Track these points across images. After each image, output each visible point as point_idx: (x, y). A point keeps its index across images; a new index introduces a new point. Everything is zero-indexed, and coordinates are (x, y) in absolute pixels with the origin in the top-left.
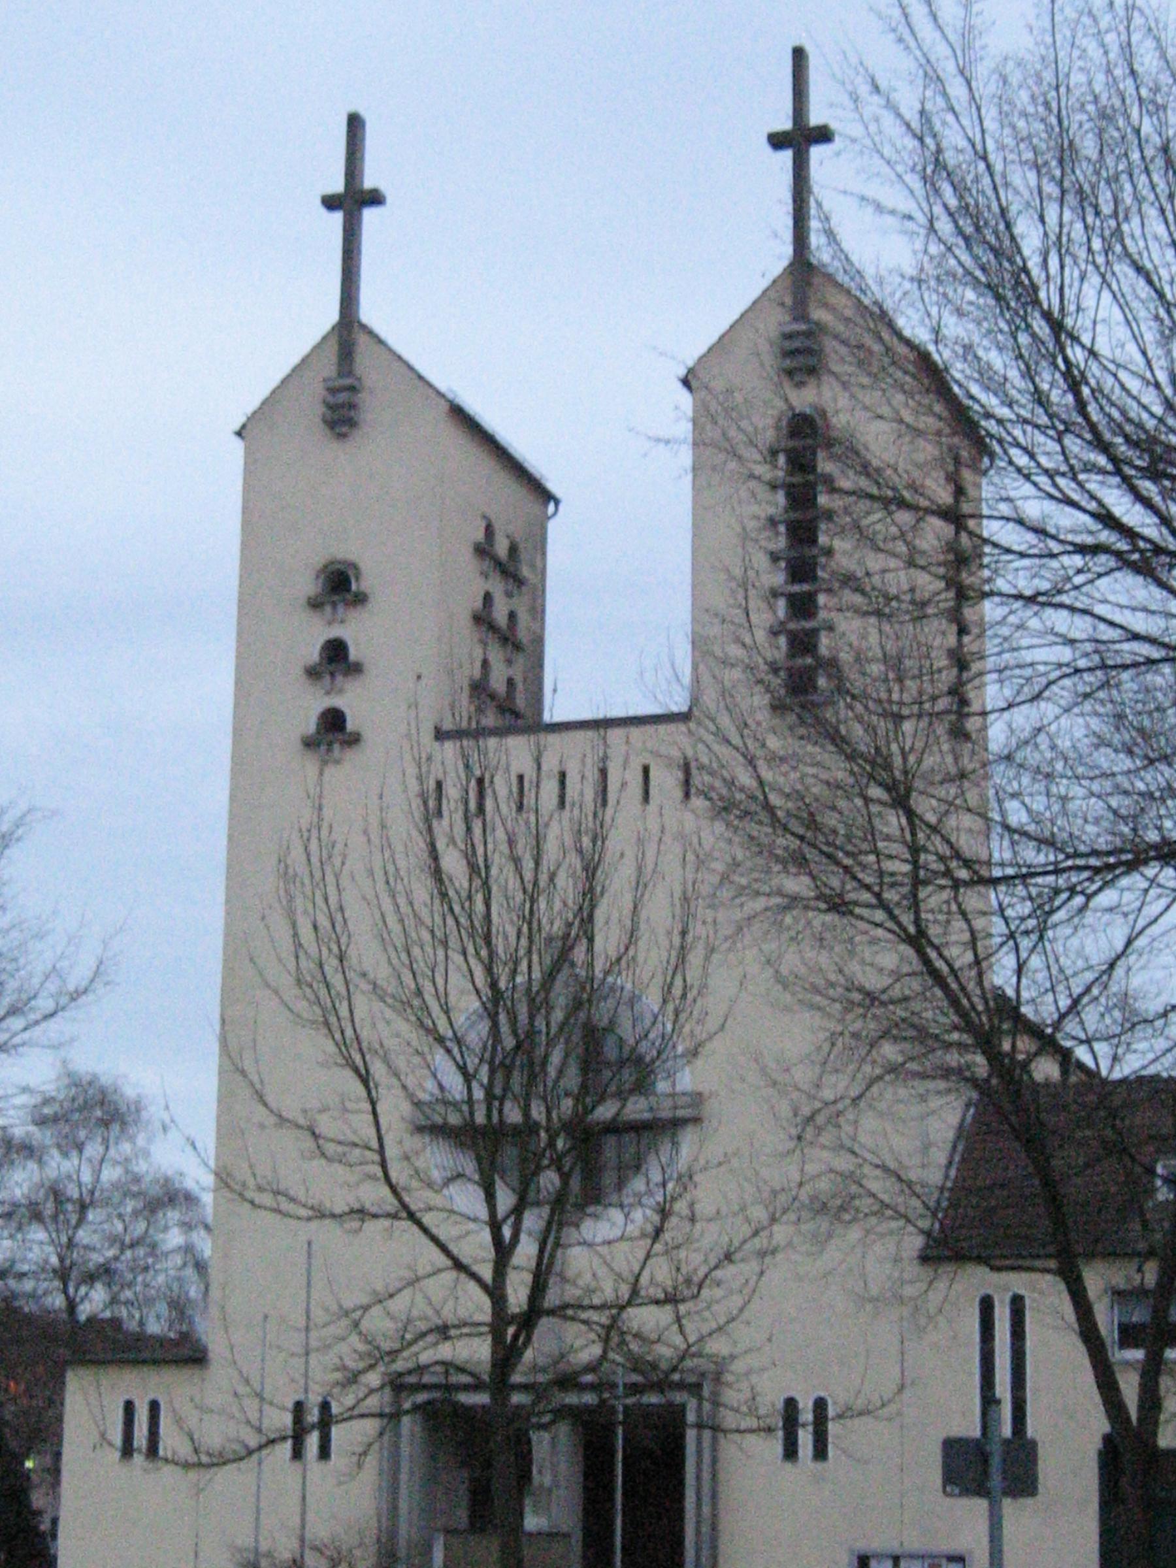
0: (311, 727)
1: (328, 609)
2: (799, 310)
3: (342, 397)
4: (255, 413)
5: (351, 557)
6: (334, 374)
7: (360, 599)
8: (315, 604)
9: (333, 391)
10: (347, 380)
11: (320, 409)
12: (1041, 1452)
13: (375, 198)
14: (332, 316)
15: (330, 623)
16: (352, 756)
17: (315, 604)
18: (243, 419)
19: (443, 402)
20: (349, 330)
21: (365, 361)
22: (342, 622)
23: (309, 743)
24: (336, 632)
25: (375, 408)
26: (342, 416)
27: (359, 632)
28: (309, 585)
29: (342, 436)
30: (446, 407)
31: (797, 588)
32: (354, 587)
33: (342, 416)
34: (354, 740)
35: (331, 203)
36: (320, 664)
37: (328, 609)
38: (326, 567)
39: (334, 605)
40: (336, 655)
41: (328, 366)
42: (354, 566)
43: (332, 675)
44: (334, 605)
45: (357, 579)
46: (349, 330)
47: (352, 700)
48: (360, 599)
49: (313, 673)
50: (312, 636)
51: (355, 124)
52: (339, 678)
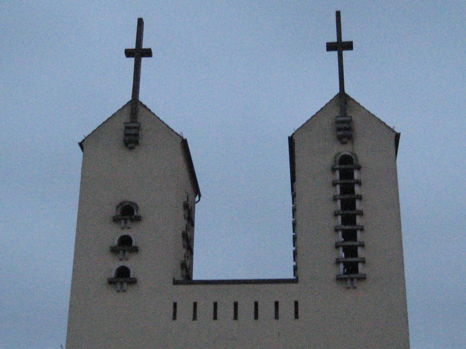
0: (113, 274)
1: (123, 222)
2: (343, 112)
3: (133, 132)
4: (89, 135)
5: (134, 201)
6: (129, 121)
7: (138, 219)
8: (116, 220)
9: (127, 128)
10: (133, 126)
11: (121, 134)
12: (125, 55)
13: (148, 53)
14: (128, 97)
15: (123, 228)
16: (131, 290)
17: (116, 220)
18: (83, 138)
19: (179, 138)
20: (135, 105)
21: (142, 118)
22: (129, 228)
23: (111, 282)
24: (125, 232)
25: (146, 137)
26: (131, 139)
27: (135, 233)
28: (112, 211)
29: (131, 148)
30: (181, 140)
31: (348, 227)
32: (135, 214)
33: (131, 139)
34: (133, 282)
35: (129, 53)
36: (115, 278)
37: (119, 286)
38: (121, 204)
39: (122, 283)
40: (126, 245)
41: (126, 118)
42: (136, 206)
43: (126, 220)
44: (122, 283)
45: (137, 210)
46: (135, 105)
47: (133, 263)
48: (138, 219)
49: (114, 250)
50: (114, 234)
51: (140, 22)
52: (127, 253)
